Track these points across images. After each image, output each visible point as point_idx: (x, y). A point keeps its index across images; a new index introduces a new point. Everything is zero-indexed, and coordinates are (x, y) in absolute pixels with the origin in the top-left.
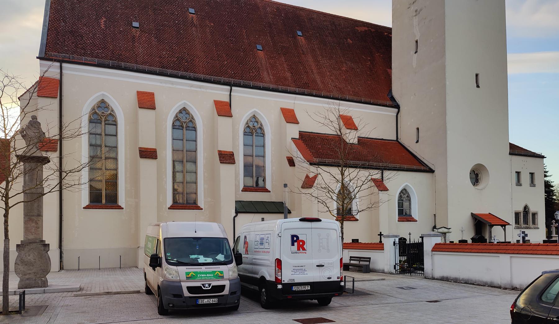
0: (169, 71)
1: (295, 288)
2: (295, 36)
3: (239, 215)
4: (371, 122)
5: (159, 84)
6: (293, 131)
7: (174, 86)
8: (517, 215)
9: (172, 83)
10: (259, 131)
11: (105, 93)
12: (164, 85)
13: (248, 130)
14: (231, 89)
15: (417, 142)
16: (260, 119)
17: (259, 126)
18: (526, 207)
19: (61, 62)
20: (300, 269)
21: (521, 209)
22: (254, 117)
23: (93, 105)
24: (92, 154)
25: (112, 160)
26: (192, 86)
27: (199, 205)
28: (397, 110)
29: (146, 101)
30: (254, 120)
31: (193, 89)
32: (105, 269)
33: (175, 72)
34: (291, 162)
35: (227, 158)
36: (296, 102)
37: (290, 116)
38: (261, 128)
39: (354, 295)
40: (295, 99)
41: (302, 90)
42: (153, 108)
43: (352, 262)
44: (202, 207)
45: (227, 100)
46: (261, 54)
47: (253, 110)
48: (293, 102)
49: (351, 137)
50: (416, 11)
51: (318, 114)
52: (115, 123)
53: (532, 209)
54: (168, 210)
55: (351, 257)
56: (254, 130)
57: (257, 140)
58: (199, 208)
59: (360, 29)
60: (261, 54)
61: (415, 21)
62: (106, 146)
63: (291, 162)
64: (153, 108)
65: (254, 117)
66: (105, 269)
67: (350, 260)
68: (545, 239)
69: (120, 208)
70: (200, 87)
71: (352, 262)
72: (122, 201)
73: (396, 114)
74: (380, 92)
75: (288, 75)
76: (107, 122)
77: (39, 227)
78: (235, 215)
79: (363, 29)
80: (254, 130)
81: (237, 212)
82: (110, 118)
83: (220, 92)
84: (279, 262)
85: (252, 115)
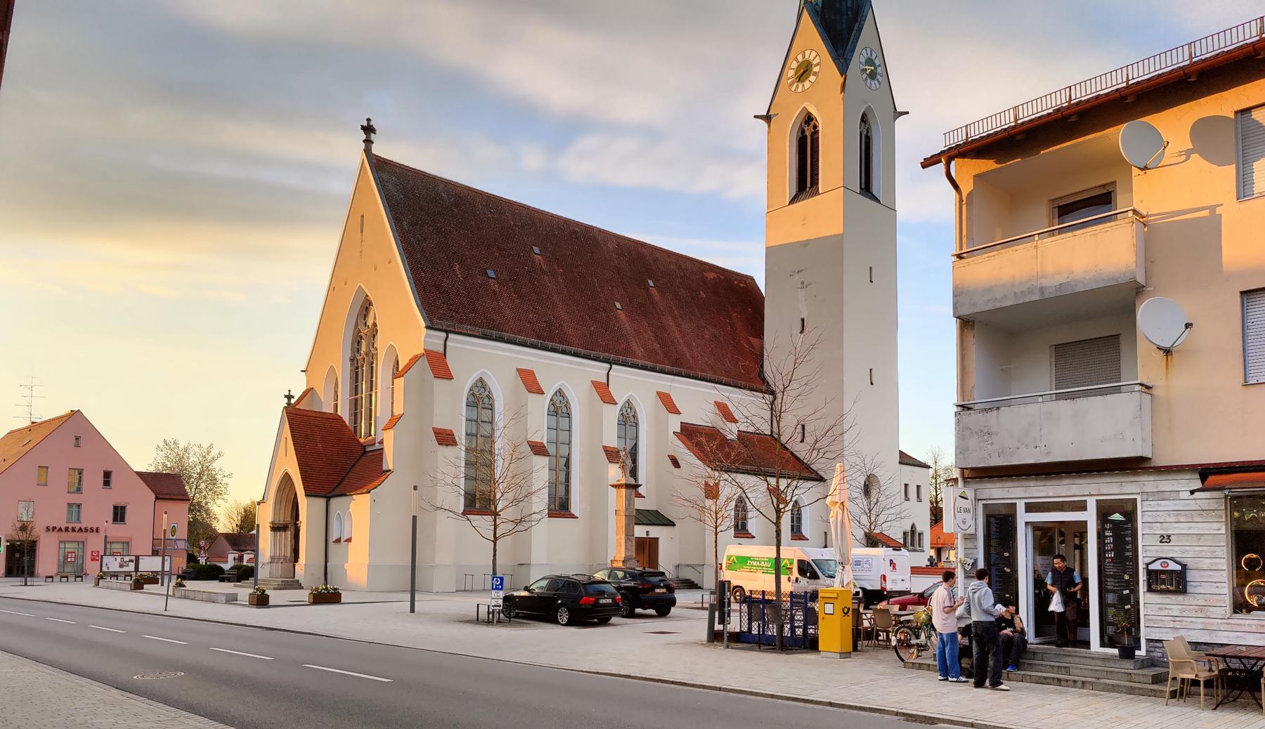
0: (520, 338)
1: (652, 612)
2: (647, 288)
4: (749, 411)
6: (674, 424)
8: (905, 533)
10: (486, 401)
13: (472, 399)
15: (802, 441)
18: (913, 526)
20: (894, 581)
21: (908, 529)
22: (481, 380)
26: (571, 363)
29: (603, 391)
33: (556, 345)
34: (676, 464)
35: (445, 438)
37: (668, 403)
38: (489, 397)
40: (672, 381)
42: (451, 378)
45: (441, 350)
46: (621, 314)
49: (731, 431)
51: (699, 400)
53: (919, 529)
56: (480, 399)
57: (564, 422)
58: (573, 516)
60: (621, 314)
63: (676, 464)
64: (451, 378)
65: (481, 380)
69: (573, 516)
72: (575, 508)
74: (751, 375)
75: (656, 345)
79: (711, 275)
82: (486, 401)
83: (597, 370)
84: (884, 577)
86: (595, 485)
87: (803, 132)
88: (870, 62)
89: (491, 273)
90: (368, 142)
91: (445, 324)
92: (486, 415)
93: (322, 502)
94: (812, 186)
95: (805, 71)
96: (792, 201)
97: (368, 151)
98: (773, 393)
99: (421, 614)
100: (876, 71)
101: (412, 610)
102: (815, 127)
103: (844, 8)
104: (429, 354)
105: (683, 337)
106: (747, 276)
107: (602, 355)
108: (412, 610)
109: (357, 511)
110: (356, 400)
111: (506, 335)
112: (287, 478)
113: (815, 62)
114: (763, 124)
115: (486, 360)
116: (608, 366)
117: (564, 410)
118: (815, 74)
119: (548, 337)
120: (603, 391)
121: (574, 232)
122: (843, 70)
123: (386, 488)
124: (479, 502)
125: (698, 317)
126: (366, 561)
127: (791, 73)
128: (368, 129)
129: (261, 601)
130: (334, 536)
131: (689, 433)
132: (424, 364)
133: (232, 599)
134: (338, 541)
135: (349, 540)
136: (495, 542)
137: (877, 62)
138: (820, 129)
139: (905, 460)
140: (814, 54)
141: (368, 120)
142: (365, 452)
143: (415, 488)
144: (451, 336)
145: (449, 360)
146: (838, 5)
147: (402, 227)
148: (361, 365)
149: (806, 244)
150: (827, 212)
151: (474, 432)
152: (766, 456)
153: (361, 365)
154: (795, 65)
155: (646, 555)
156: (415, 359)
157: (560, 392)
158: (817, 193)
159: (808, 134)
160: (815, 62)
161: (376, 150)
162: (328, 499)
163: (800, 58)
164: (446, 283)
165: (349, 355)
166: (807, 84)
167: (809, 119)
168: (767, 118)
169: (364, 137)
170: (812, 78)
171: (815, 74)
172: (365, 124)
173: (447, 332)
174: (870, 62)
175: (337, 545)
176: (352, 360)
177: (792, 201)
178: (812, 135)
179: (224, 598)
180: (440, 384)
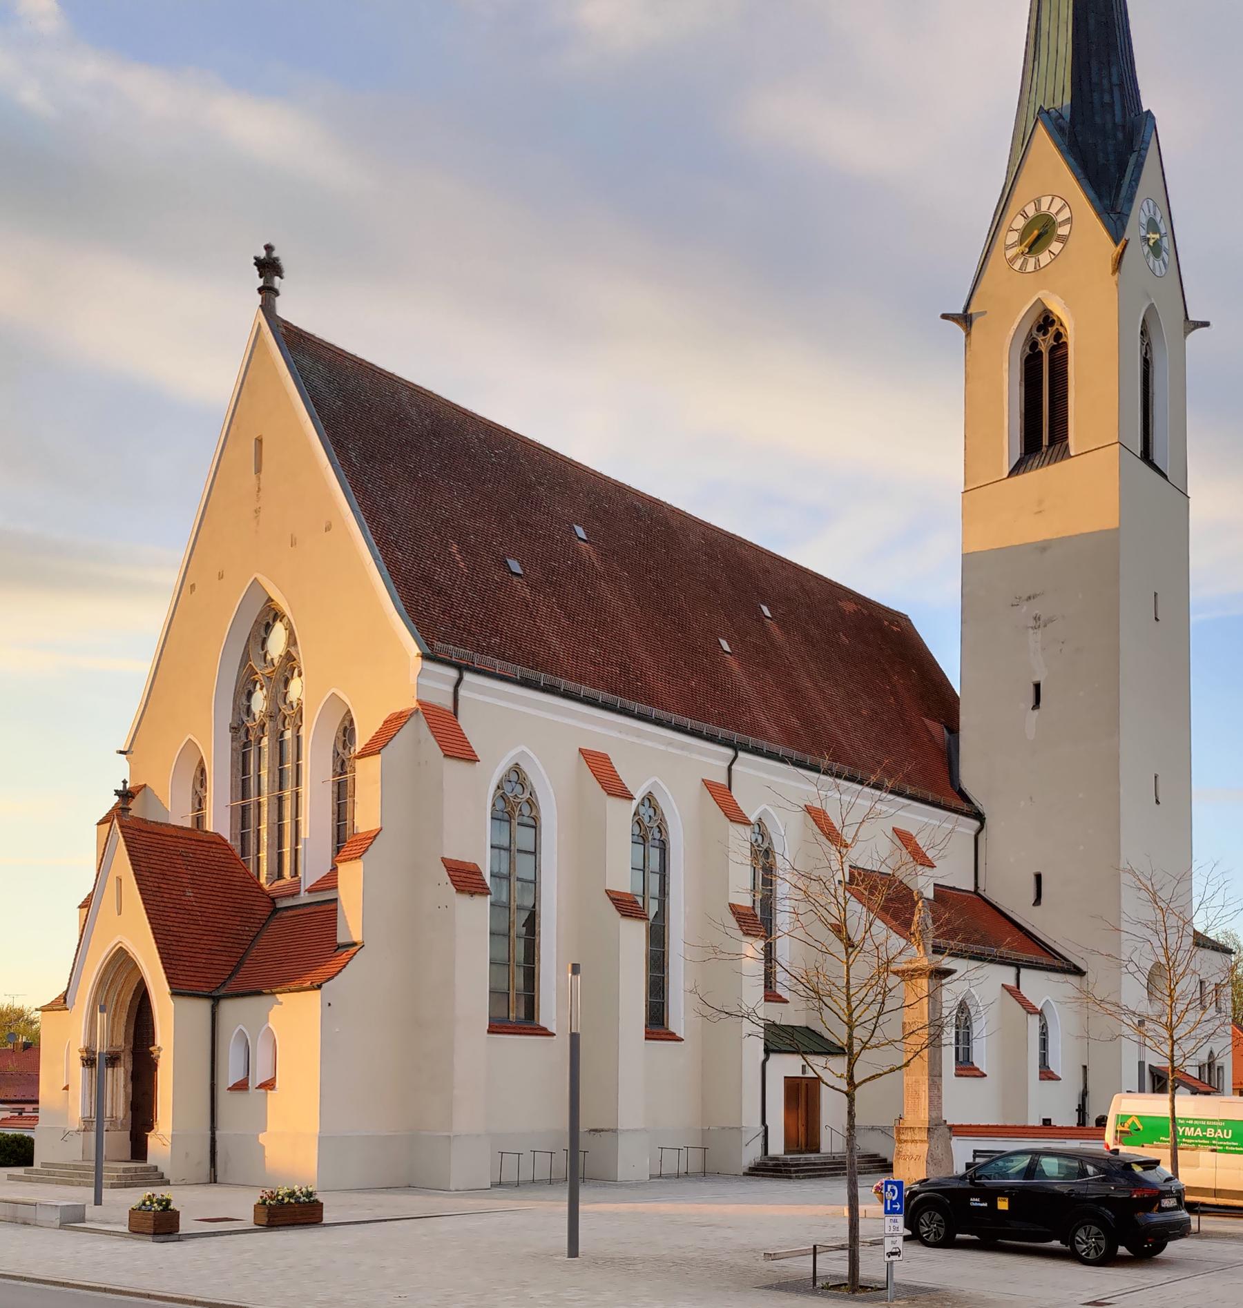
3: (773, 1057)
16: (661, 804)
17: (765, 845)
19: (737, 747)
22: (516, 769)
27: (672, 1029)
28: (977, 824)
32: (668, 1177)
38: (532, 803)
41: (689, 723)
45: (448, 703)
47: (513, 753)
50: (1037, 618)
51: (877, 823)
52: (532, 822)
55: (975, 1151)
56: (515, 806)
58: (673, 1037)
59: (849, 607)
62: (519, 879)
65: (516, 769)
66: (668, 1177)
67: (974, 1157)
68: (172, 1207)
69: (673, 1037)
70: (684, 747)
71: (978, 1160)
73: (451, 690)
75: (795, 722)
78: (762, 1056)
80: (515, 806)
81: (767, 1051)
83: (710, 759)
85: (511, 765)
86: (719, 975)
87: (1034, 345)
88: (1152, 226)
89: (515, 566)
90: (268, 291)
91: (455, 652)
92: (524, 838)
93: (201, 1008)
94: (1052, 442)
95: (1040, 234)
96: (1016, 470)
97: (268, 308)
98: (979, 816)
99: (620, 1264)
100: (1162, 245)
101: (573, 1251)
102: (1058, 336)
103: (1109, 126)
104: (427, 710)
105: (831, 710)
106: (898, 614)
107: (722, 732)
108: (573, 1251)
109: (292, 1027)
110: (245, 809)
111: (564, 683)
112: (121, 961)
113: (1060, 218)
114: (957, 330)
115: (530, 729)
116: (730, 752)
117: (657, 836)
118: (1063, 239)
119: (624, 693)
120: (721, 795)
121: (637, 510)
122: (1117, 233)
123: (352, 978)
124: (516, 1013)
125: (837, 680)
126: (312, 1126)
127: (1013, 237)
128: (268, 267)
129: (161, 1223)
130: (231, 1073)
131: (862, 882)
132: (420, 729)
133: (72, 1219)
134: (242, 1086)
135: (269, 1085)
136: (850, 1096)
137: (1163, 228)
138: (1071, 339)
139: (1201, 941)
140: (1058, 203)
141: (269, 248)
142: (276, 910)
143: (576, 969)
144: (468, 677)
145: (462, 721)
146: (1098, 120)
147: (351, 464)
148: (259, 738)
149: (1043, 547)
150: (1086, 486)
151: (504, 869)
152: (977, 927)
153: (259, 738)
154: (1020, 223)
155: (802, 1112)
156: (395, 723)
157: (649, 799)
158: (1065, 454)
159: (1044, 348)
160: (1060, 218)
161: (288, 309)
162: (216, 1000)
163: (1031, 211)
164: (440, 576)
165: (228, 718)
166: (1045, 258)
167: (1046, 321)
168: (965, 319)
169: (260, 282)
170: (1056, 247)
171: (1063, 239)
172: (262, 254)
173: (460, 668)
174: (1152, 226)
175: (238, 1095)
176: (234, 729)
177: (1016, 470)
178: (1053, 350)
179: (55, 1217)
180: (454, 769)
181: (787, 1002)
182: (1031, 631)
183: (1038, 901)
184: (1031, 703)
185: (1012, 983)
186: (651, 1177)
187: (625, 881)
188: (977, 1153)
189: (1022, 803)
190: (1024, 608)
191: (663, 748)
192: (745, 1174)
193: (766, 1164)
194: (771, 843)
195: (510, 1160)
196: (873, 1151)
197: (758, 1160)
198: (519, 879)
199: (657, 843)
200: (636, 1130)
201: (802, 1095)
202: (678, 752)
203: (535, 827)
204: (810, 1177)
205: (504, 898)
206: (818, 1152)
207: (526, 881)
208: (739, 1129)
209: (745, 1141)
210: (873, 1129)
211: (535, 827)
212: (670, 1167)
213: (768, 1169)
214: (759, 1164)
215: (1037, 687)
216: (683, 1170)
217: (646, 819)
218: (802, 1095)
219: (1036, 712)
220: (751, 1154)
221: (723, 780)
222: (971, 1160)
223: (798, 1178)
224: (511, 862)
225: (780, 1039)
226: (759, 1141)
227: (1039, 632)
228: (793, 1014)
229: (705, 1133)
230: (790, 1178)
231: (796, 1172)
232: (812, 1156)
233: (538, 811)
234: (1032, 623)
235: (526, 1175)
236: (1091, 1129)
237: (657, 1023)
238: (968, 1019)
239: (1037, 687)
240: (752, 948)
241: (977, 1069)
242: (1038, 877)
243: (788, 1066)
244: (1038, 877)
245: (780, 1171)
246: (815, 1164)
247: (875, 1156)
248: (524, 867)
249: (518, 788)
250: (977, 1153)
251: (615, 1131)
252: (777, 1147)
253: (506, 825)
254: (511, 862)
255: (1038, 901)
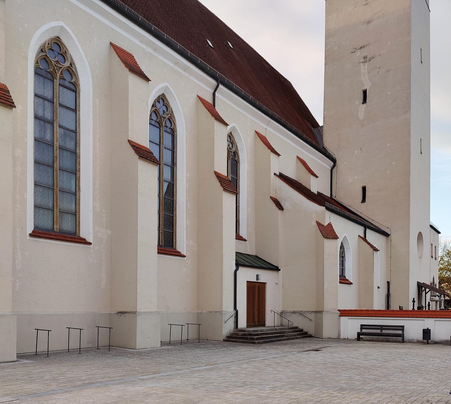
3: (241, 269)
5: (138, 42)
7: (156, 54)
9: (156, 49)
10: (67, 76)
11: (169, 87)
12: (144, 46)
13: (43, 65)
14: (217, 86)
17: (67, 64)
23: (43, 41)
24: (37, 136)
25: (69, 154)
30: (56, 48)
31: (177, 68)
36: (268, 128)
39: (428, 345)
43: (364, 331)
44: (90, 239)
48: (265, 126)
50: (365, 57)
54: (28, 238)
55: (362, 326)
61: (364, 68)
67: (361, 329)
71: (364, 331)
76: (62, 82)
77: (421, 303)
78: (234, 268)
98: (334, 161)
117: (168, 124)
181: (245, 240)
182: (362, 64)
183: (364, 200)
184: (362, 101)
185: (362, 235)
186: (163, 344)
187: (143, 134)
188: (362, 327)
189: (356, 152)
190: (358, 53)
191: (172, 65)
192: (224, 340)
193: (237, 334)
194: (237, 148)
195: (75, 333)
196: (295, 325)
197: (232, 331)
198: (60, 126)
199: (169, 130)
200: (151, 312)
201: (256, 292)
202: (182, 71)
203: (75, 92)
204: (266, 342)
205: (48, 137)
206: (264, 325)
207: (68, 129)
208: (221, 312)
209: (224, 320)
210: (294, 312)
211: (75, 92)
212: (176, 337)
213: (238, 338)
214: (232, 334)
215: (365, 92)
216: (185, 337)
217: (161, 113)
218: (256, 292)
219: (365, 105)
220: (228, 328)
221: (210, 100)
222: (359, 331)
223: (259, 343)
224: (54, 112)
225: (243, 261)
226: (233, 320)
227: (366, 64)
228: (248, 249)
229: (199, 315)
230: (254, 343)
231: (257, 339)
232: (262, 328)
233: (77, 79)
234: (362, 60)
235: (74, 345)
236: (416, 311)
237: (167, 244)
238: (344, 251)
239: (365, 92)
240: (228, 199)
241: (348, 280)
242: (364, 189)
243: (247, 275)
244: (364, 189)
245: (247, 339)
246: (267, 334)
247: (296, 328)
248: (64, 118)
249: (60, 58)
250: (362, 327)
251: (135, 313)
252: (243, 323)
253: (49, 83)
254: (54, 112)
255: (364, 200)
